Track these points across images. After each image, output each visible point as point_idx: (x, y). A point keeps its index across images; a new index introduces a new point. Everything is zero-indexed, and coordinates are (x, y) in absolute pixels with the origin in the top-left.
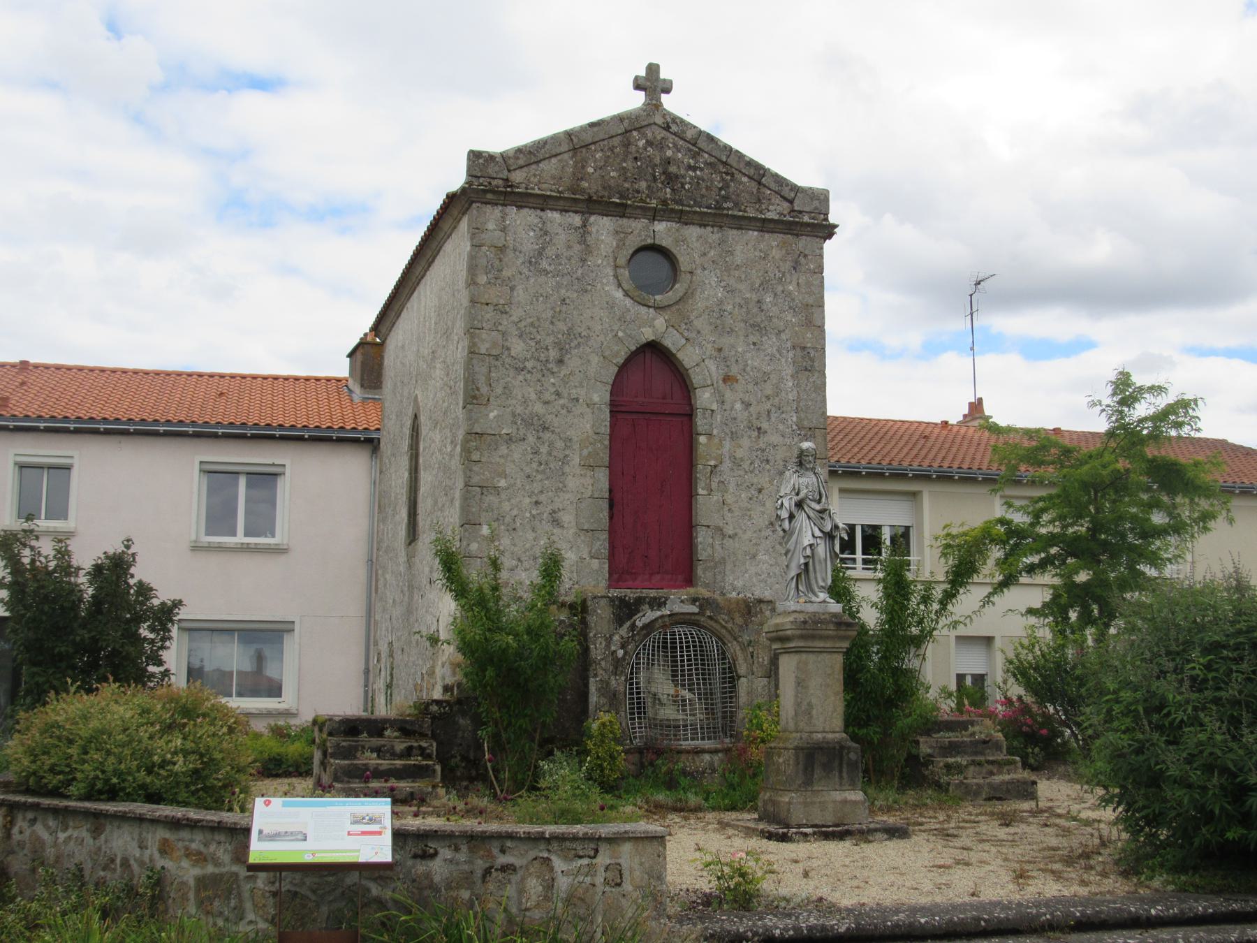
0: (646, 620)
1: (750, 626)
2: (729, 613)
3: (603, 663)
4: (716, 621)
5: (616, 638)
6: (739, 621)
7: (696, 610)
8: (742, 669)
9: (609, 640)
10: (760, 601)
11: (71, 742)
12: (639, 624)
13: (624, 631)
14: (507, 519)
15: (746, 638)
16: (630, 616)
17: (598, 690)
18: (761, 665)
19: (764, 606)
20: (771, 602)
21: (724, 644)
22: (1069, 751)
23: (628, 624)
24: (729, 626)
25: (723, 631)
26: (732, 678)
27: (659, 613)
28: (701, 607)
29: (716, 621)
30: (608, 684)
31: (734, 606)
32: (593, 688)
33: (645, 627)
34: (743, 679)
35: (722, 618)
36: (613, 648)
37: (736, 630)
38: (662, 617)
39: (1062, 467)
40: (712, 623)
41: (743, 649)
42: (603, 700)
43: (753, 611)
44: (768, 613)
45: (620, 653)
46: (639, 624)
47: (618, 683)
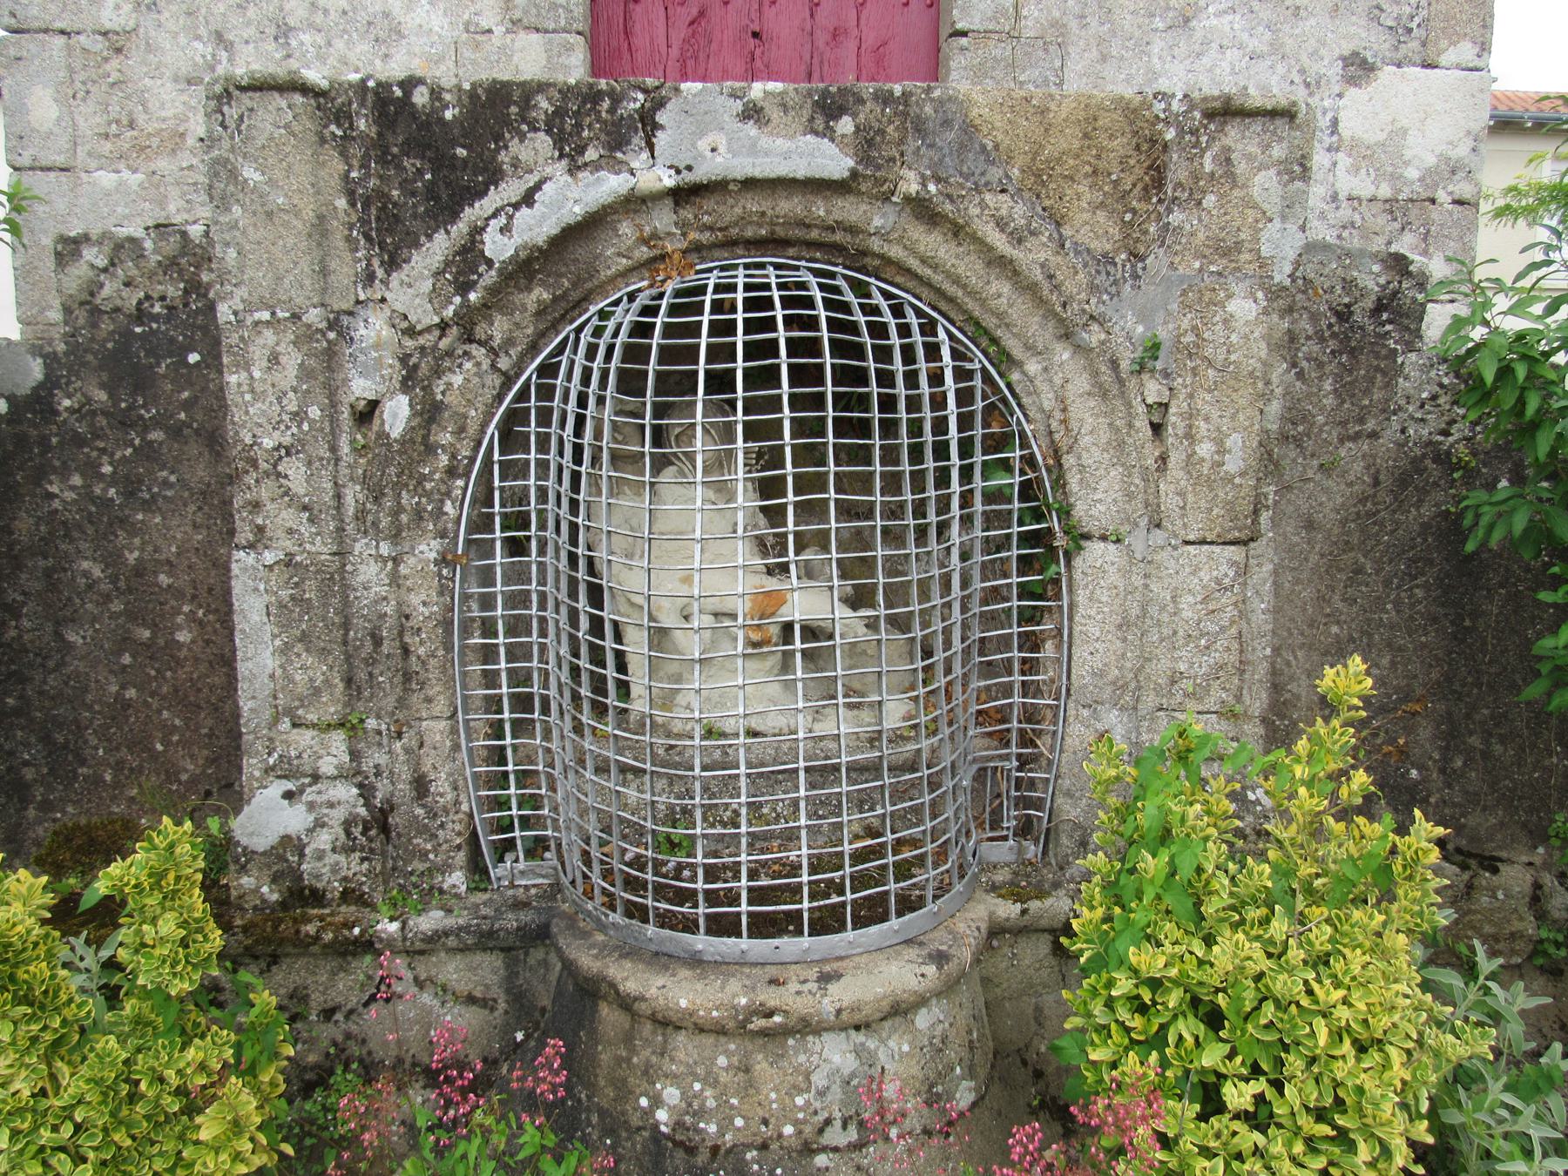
0: (537, 226)
1: (1157, 260)
2: (1039, 180)
3: (294, 469)
4: (958, 231)
5: (373, 329)
6: (1093, 228)
7: (833, 161)
8: (1096, 494)
9: (329, 346)
10: (1226, 112)
11: (257, 481)
12: (499, 247)
13: (415, 290)
14: (241, 196)
15: (1129, 326)
16: (448, 199)
17: (281, 614)
18: (1207, 479)
19: (1240, 140)
20: (1286, 113)
21: (1005, 360)
22: (28, 352)
23: (439, 247)
24: (1033, 256)
25: (1000, 289)
26: (1041, 545)
27: (612, 185)
28: (866, 143)
29: (958, 231)
30: (337, 579)
31: (1069, 140)
32: (252, 606)
33: (527, 267)
34: (1095, 552)
35: (988, 213)
36: (361, 388)
37: (1075, 284)
38: (634, 203)
39: (407, 485)
40: (932, 242)
41: (1112, 381)
42: (310, 669)
43: (1178, 170)
44: (1265, 185)
45: (397, 414)
46: (499, 247)
47: (398, 578)
